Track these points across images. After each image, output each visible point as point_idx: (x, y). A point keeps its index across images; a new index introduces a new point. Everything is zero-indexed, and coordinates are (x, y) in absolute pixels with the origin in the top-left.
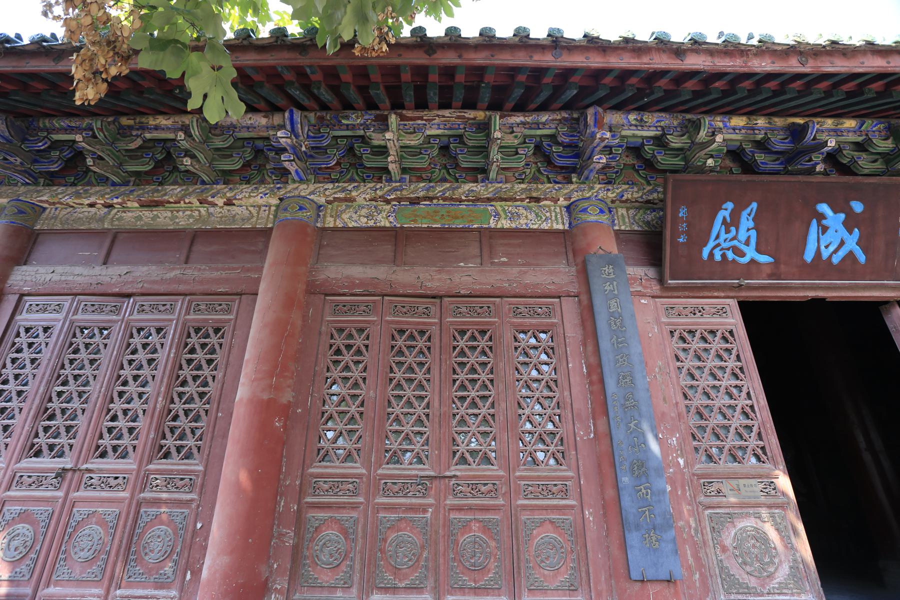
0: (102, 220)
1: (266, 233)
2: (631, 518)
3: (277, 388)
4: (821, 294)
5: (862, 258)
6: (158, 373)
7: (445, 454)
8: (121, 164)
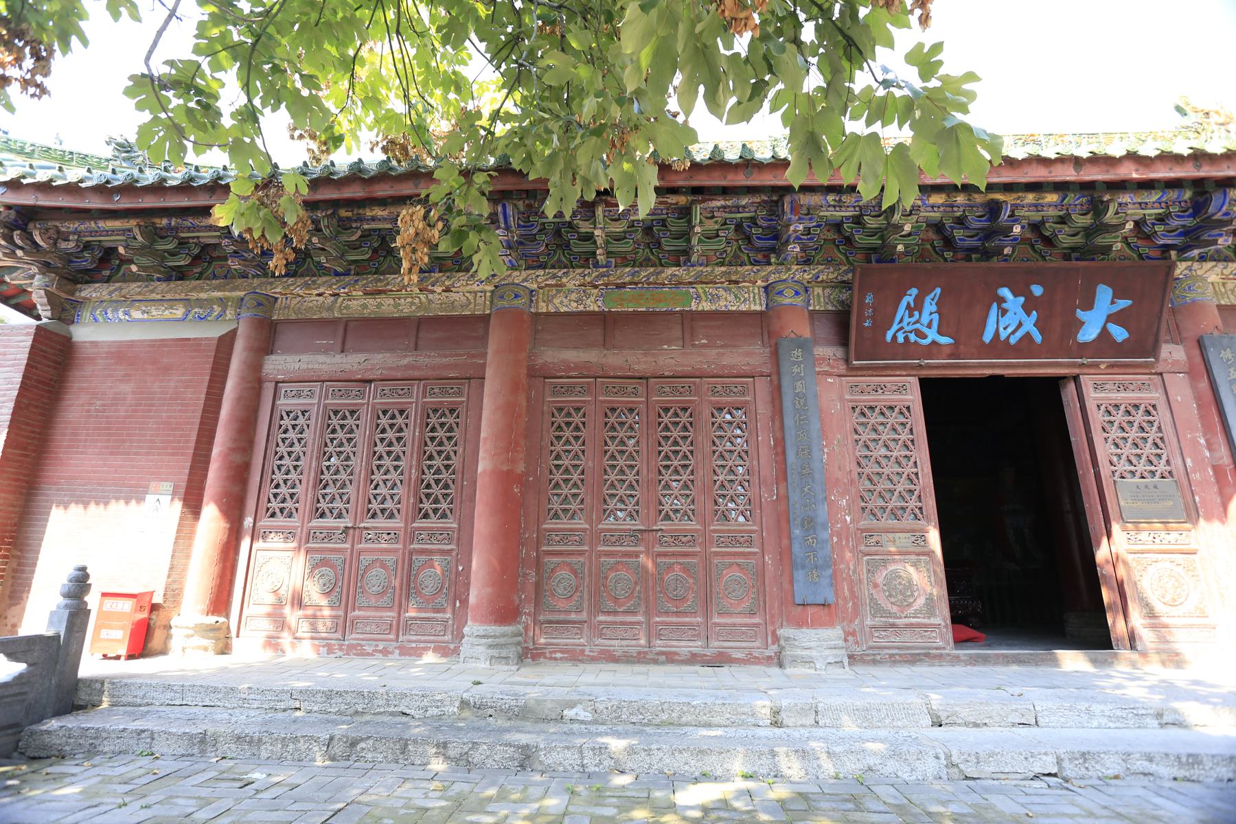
0: (330, 309)
1: (485, 319)
2: (799, 561)
3: (513, 461)
4: (998, 372)
5: (1038, 338)
6: (408, 449)
7: (652, 513)
8: (343, 255)
